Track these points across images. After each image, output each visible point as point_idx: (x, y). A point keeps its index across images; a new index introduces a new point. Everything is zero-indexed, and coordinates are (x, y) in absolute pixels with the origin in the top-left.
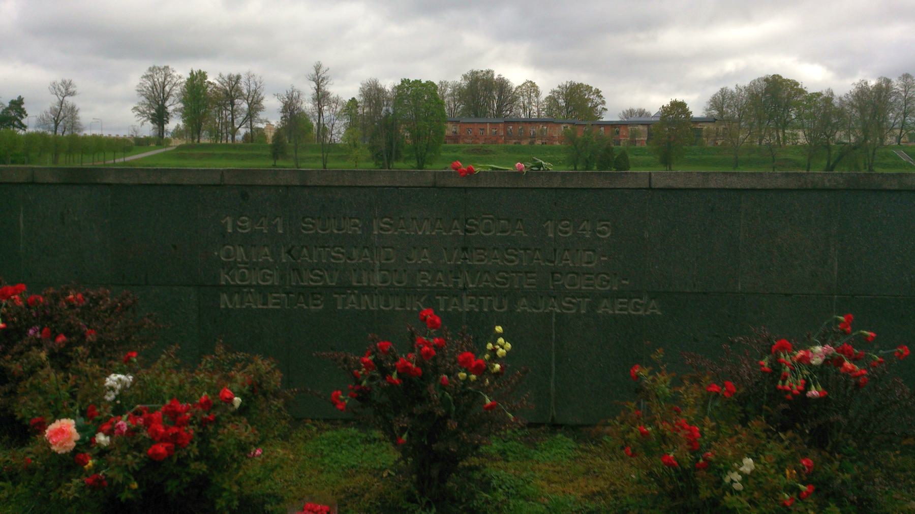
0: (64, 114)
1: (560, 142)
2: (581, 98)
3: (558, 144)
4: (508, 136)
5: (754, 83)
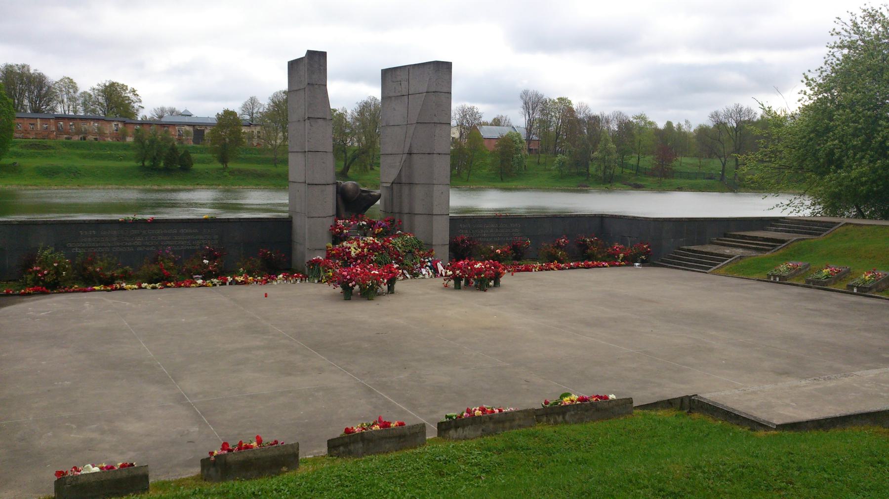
4: (60, 131)
5: (276, 95)
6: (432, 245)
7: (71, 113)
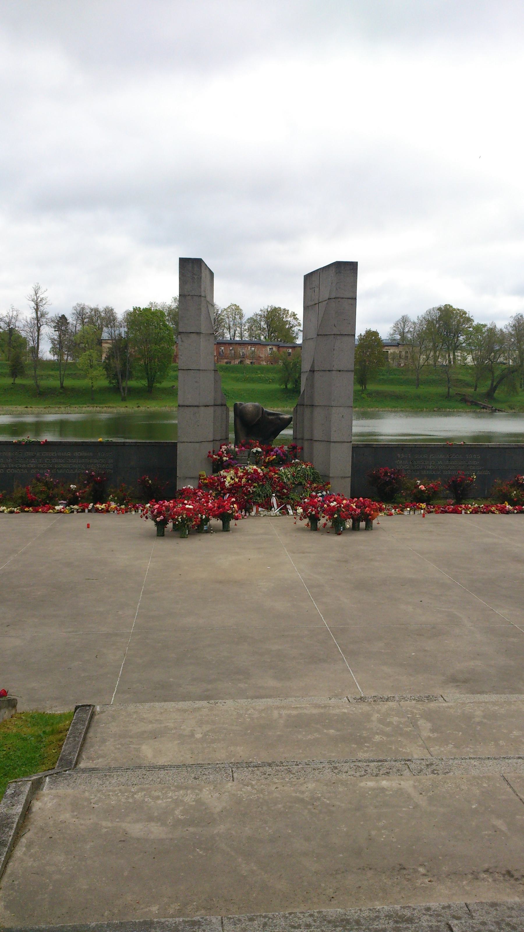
1: (267, 362)
2: (280, 320)
3: (264, 363)
5: (429, 312)
6: (328, 477)
7: (237, 339)
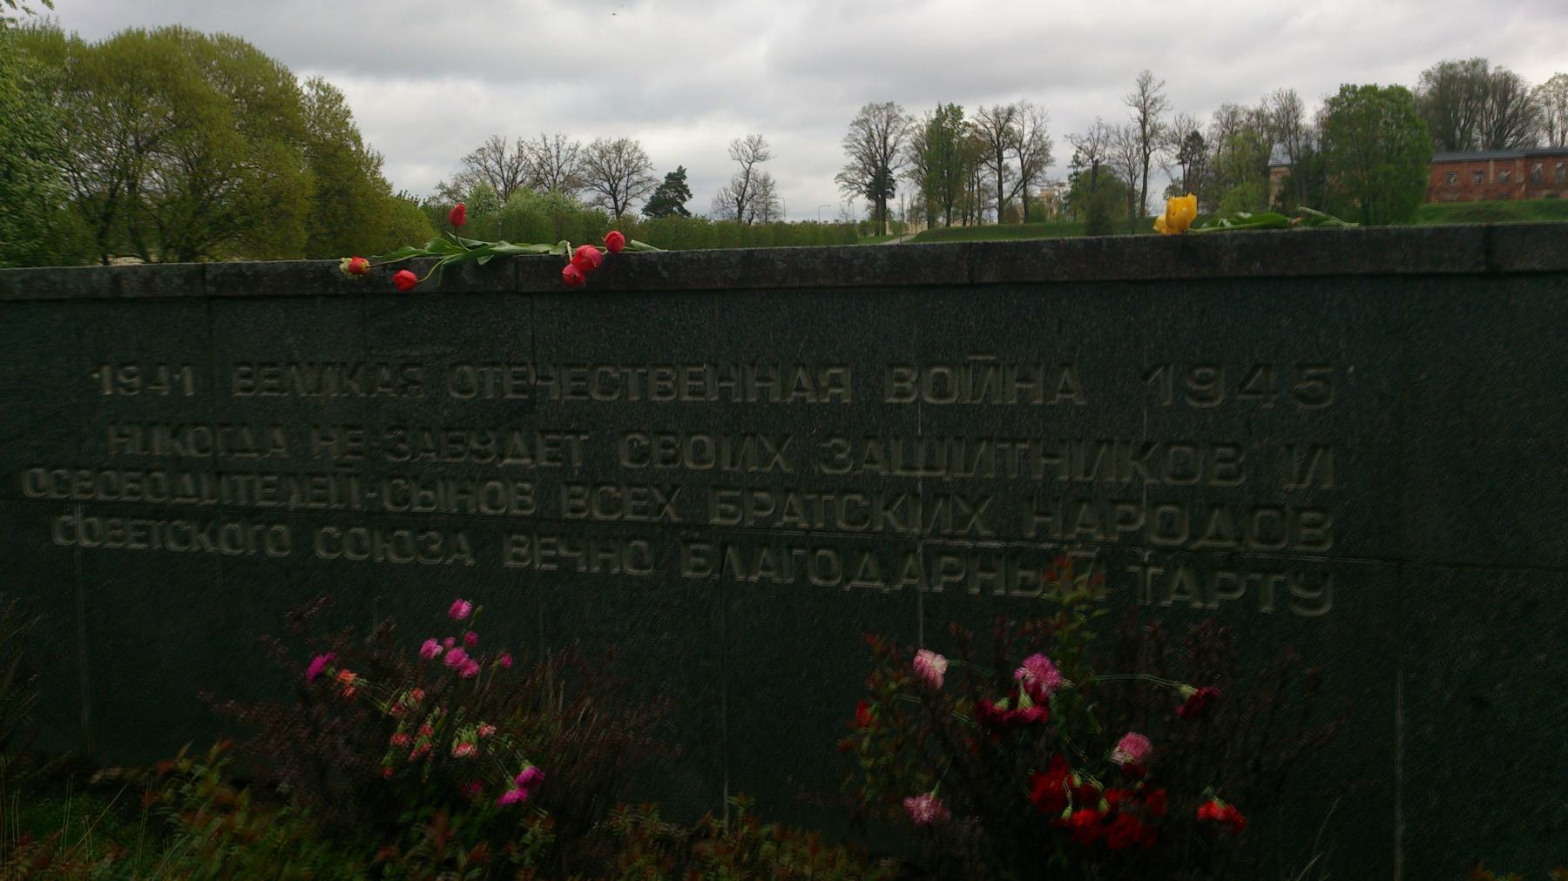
0: (752, 190)
4: (1533, 183)
